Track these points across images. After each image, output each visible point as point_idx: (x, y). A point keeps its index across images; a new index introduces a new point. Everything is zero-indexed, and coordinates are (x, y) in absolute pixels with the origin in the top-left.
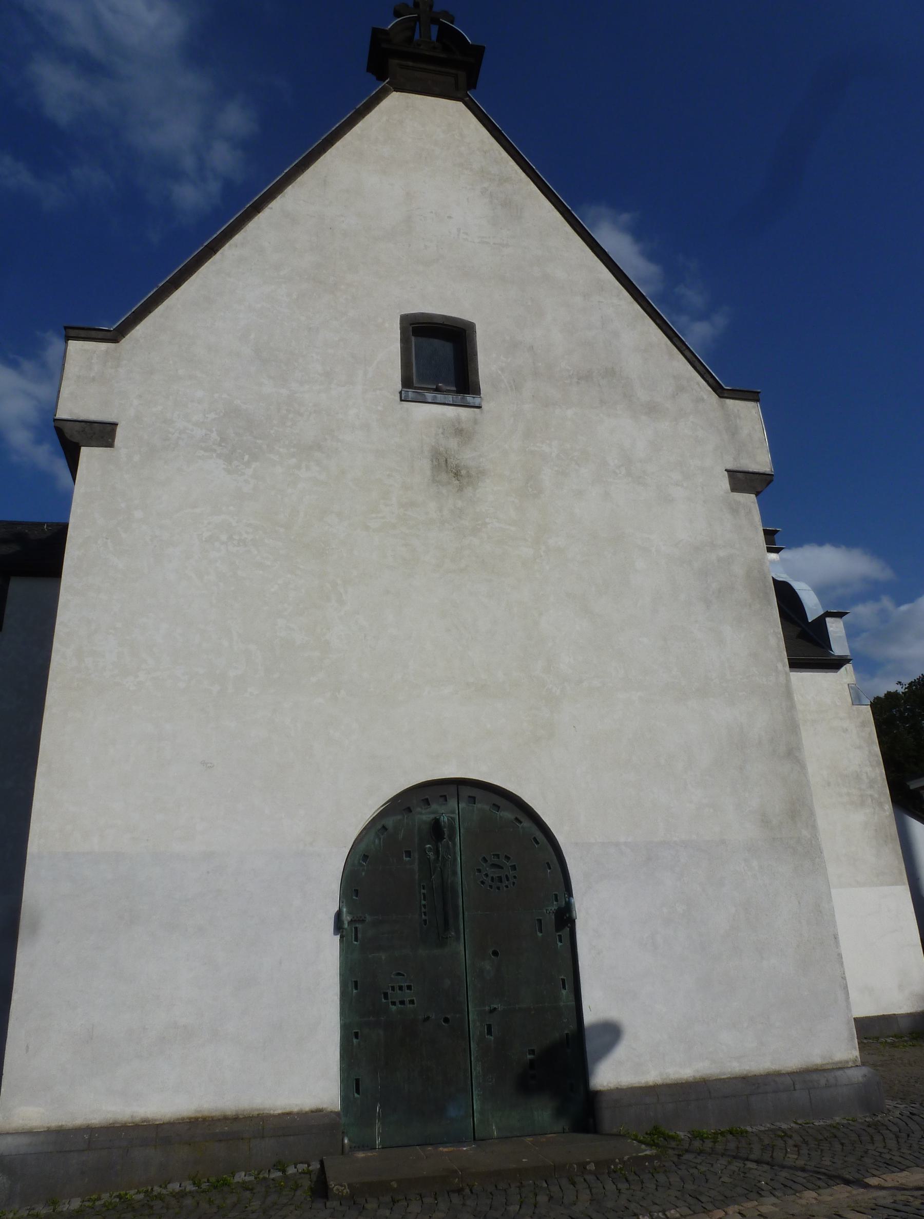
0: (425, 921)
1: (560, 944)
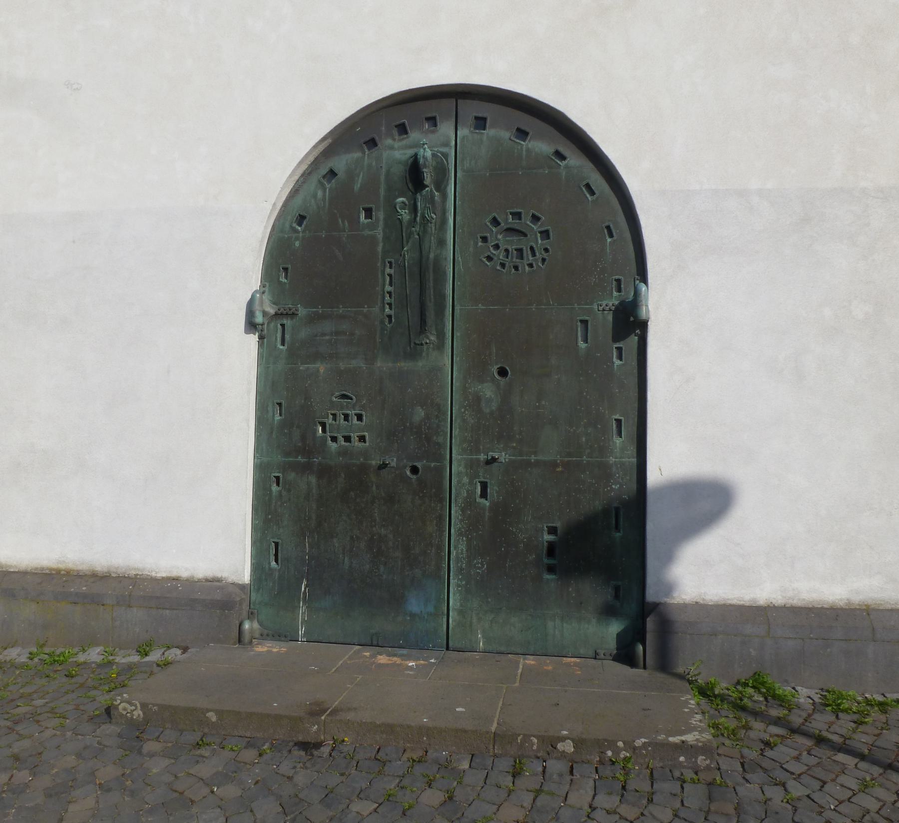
0: (390, 317)
1: (617, 362)
